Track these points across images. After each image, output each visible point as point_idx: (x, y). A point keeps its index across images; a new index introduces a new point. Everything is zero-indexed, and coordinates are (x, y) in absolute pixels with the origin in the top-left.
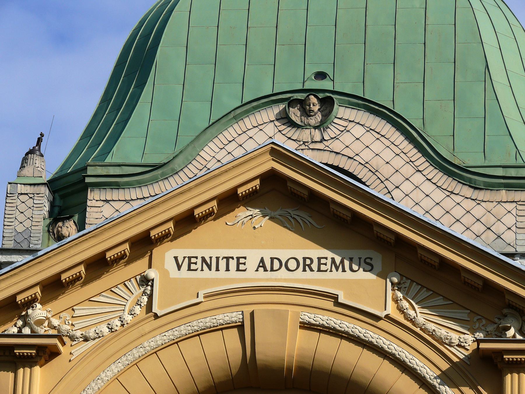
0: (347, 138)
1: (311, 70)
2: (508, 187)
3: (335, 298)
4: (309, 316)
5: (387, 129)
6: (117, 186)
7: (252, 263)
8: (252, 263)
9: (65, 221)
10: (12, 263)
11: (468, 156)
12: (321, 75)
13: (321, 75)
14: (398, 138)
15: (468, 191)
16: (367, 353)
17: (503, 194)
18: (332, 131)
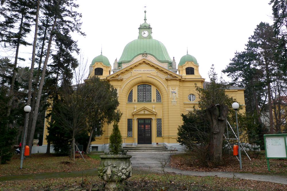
0: (148, 58)
1: (144, 51)
2: (165, 63)
3: (151, 74)
4: (148, 76)
5: (153, 57)
6: (125, 63)
7: (142, 71)
8: (142, 71)
9: (11, 28)
10: (75, 145)
11: (161, 59)
12: (145, 51)
13: (145, 51)
14: (154, 58)
15: (161, 63)
16: (152, 79)
17: (165, 63)
18: (147, 57)
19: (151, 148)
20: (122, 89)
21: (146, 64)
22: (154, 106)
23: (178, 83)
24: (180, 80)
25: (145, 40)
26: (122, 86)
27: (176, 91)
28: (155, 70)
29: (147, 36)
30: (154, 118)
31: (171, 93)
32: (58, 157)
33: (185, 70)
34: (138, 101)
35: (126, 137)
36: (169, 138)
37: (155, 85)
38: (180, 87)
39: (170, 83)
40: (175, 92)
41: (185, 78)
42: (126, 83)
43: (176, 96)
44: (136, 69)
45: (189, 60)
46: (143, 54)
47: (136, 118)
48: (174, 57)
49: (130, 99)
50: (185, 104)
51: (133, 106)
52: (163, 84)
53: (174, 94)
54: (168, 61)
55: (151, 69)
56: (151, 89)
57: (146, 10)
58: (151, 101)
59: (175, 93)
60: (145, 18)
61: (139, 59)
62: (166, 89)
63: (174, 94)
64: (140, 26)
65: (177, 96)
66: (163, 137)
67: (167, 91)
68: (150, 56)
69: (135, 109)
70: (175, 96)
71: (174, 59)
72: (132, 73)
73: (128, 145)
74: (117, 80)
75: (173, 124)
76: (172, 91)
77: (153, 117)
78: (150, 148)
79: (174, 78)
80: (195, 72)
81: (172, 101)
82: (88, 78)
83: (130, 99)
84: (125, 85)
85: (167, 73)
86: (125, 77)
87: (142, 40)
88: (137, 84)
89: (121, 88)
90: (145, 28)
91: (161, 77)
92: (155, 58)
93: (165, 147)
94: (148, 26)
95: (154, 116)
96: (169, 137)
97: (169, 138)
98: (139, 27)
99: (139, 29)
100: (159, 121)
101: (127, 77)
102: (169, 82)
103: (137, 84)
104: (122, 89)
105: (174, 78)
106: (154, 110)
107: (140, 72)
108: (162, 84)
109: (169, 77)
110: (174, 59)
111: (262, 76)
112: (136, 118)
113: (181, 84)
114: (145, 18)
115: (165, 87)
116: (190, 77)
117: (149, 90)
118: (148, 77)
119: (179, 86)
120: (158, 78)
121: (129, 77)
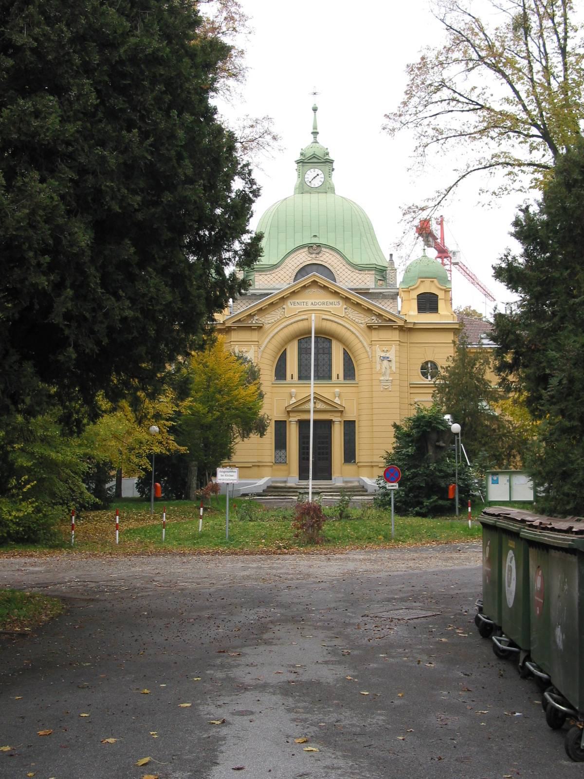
7: (309, 304)
8: (309, 304)
11: (357, 260)
12: (315, 236)
14: (338, 256)
15: (357, 271)
18: (321, 255)
19: (331, 488)
20: (262, 349)
21: (320, 287)
22: (337, 390)
23: (395, 335)
24: (401, 329)
25: (314, 196)
26: (260, 343)
27: (392, 355)
28: (341, 302)
29: (321, 184)
30: (339, 419)
31: (378, 359)
32: (404, 518)
33: (416, 301)
34: (300, 378)
35: (271, 464)
36: (372, 466)
37: (340, 340)
38: (401, 344)
39: (375, 335)
40: (388, 358)
41: (415, 323)
42: (271, 335)
43: (391, 367)
44: (297, 301)
45: (424, 275)
46: (310, 247)
47: (294, 418)
48: (391, 255)
49: (280, 372)
50: (413, 386)
51: (287, 390)
52: (361, 338)
53: (385, 362)
54: (375, 266)
55: (331, 301)
56: (330, 347)
57: (317, 106)
58: (330, 378)
59: (390, 361)
60: (315, 128)
61: (298, 259)
62: (368, 349)
63: (385, 362)
64: (302, 154)
65: (394, 368)
66: (359, 464)
67: (370, 354)
68: (327, 250)
69: (292, 397)
70: (388, 367)
71: (391, 260)
72: (284, 308)
73: (277, 482)
74: (250, 328)
75: (377, 443)
76: (383, 354)
77: (336, 418)
78: (327, 488)
79: (386, 324)
80: (441, 305)
81: (382, 378)
82: (519, 673)
83: (280, 372)
84: (267, 340)
85: (371, 310)
86: (267, 319)
87: (306, 196)
88: (297, 336)
89: (259, 346)
90: (315, 160)
91: (357, 320)
92: (341, 259)
93: (363, 487)
94: (319, 153)
95: (339, 414)
96: (373, 464)
97: (372, 466)
98: (298, 157)
99: (298, 162)
100: (350, 427)
101: (273, 321)
102: (374, 333)
103: (297, 336)
104: (262, 349)
105: (386, 324)
106: (337, 400)
107: (305, 307)
108: (357, 337)
109: (375, 321)
110: (391, 260)
111: (524, 387)
112: (296, 419)
113: (405, 337)
114: (315, 128)
115: (365, 344)
116: (428, 318)
117: (326, 351)
118: (323, 319)
119: (398, 342)
120: (350, 324)
121: (279, 320)
